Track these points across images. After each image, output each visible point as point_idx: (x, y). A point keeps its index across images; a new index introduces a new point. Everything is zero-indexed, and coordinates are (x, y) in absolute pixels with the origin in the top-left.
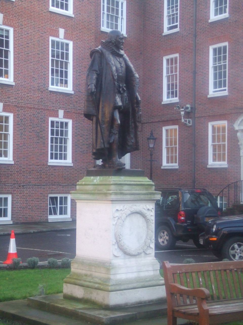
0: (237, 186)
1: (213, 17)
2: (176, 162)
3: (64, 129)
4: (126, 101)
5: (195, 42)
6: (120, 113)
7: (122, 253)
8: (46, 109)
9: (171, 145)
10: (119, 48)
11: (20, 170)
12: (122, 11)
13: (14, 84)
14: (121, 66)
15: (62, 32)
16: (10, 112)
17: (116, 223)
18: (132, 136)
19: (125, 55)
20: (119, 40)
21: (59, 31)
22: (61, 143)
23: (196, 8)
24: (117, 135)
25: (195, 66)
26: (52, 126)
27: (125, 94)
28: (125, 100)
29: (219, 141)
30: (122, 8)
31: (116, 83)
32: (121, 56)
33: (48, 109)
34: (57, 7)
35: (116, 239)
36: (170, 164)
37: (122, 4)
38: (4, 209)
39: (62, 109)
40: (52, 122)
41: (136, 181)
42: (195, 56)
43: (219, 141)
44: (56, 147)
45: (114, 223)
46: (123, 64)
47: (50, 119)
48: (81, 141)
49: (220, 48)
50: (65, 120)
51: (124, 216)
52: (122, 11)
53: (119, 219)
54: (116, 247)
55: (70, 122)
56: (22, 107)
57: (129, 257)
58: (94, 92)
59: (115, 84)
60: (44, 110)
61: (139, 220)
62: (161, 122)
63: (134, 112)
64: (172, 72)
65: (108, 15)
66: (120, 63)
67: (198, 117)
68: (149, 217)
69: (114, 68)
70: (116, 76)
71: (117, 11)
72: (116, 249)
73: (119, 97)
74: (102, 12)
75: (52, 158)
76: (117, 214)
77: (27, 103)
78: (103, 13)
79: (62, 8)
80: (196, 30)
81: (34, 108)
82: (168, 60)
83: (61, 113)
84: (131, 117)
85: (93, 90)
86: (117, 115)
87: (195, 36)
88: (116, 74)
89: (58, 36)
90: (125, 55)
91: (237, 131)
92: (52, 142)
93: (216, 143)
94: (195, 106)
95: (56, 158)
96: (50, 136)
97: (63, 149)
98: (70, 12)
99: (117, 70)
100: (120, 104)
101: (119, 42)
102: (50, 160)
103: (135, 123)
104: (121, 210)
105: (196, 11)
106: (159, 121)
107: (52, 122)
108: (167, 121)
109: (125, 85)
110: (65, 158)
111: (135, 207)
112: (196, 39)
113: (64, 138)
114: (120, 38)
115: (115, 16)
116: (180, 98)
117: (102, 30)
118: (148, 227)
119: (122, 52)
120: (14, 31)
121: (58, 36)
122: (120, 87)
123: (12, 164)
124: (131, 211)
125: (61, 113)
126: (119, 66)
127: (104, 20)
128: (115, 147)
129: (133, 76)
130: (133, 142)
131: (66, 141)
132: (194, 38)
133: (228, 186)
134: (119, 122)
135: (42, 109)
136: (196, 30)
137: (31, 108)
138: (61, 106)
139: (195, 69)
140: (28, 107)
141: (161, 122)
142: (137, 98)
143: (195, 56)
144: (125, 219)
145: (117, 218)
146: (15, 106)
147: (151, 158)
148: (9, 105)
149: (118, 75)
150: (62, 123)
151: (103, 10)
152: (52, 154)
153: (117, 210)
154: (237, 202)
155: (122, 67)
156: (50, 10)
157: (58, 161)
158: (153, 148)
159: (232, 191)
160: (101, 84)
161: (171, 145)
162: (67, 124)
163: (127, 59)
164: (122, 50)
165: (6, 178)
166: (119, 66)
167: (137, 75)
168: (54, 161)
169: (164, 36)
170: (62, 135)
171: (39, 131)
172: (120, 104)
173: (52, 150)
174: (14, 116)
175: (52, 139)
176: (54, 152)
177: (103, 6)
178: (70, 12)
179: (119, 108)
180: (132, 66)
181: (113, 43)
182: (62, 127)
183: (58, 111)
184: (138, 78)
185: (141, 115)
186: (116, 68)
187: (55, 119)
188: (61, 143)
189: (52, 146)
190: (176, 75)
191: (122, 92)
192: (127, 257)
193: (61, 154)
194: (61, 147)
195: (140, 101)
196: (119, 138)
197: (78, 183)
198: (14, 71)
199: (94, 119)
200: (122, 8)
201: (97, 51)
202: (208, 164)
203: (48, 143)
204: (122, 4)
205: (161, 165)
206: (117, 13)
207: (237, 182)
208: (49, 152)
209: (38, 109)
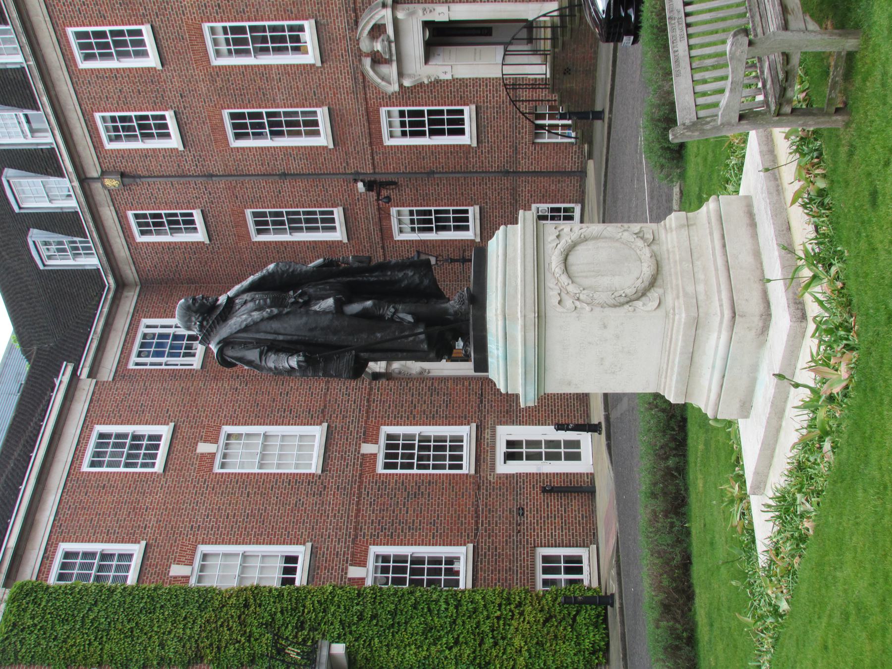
0: (513, 85)
1: (174, 142)
2: (466, 212)
3: (401, 442)
4: (326, 290)
5: (223, 176)
6: (350, 301)
7: (652, 290)
8: (360, 478)
9: (430, 221)
10: (214, 306)
11: (486, 531)
12: (163, 327)
13: (309, 545)
14: (251, 301)
15: (203, 448)
16: (366, 552)
17: (588, 304)
18: (400, 275)
19: (229, 293)
20: (197, 305)
21: (202, 454)
22: (428, 448)
23: (155, 177)
24: (397, 306)
25: (270, 175)
26: (394, 466)
27: (311, 291)
28: (323, 292)
29: (422, 124)
30: (156, 327)
31: (286, 310)
32: (231, 301)
33: (361, 475)
34: (154, 456)
35: (622, 305)
36: (471, 223)
37: (148, 327)
38: (566, 562)
39: (360, 447)
40: (387, 466)
41: (497, 272)
42: (249, 175)
43: (430, 221)
44: (436, 458)
45: (588, 308)
46: (246, 297)
47: (380, 470)
48: (425, 407)
49: (235, 126)
50: (382, 440)
51: (572, 288)
52: (163, 327)
53: (578, 299)
54: (639, 304)
55: (386, 430)
56: (356, 529)
57: (659, 277)
58: (304, 356)
59: (288, 313)
60: (361, 482)
61: (579, 258)
62: (383, 243)
63: (349, 271)
64: (282, 223)
65: (171, 355)
66: (245, 303)
67: (374, 169)
68: (574, 236)
69: (256, 315)
70: (271, 311)
71: (161, 336)
72: (644, 305)
73: (316, 304)
74: (163, 367)
75: (460, 467)
76: (569, 302)
77: (348, 518)
78: (166, 365)
79: (157, 447)
80: (198, 176)
81: (358, 503)
82: (259, 232)
83: (367, 448)
84: (361, 279)
85: (301, 358)
86: (355, 308)
87: (212, 176)
88: (268, 310)
89: (213, 455)
90: (231, 293)
91: (401, 86)
92: (426, 467)
93: (427, 129)
94: (352, 174)
95: (460, 458)
96: (415, 471)
97: (440, 444)
98: (165, 431)
99: (259, 308)
100: (330, 302)
101: (202, 305)
102: (465, 471)
103: (371, 270)
104: (559, 294)
105: (161, 177)
106: (383, 248)
107: (387, 466)
108: (381, 230)
109: (291, 293)
110: (460, 439)
111: (554, 265)
112: (217, 176)
113: (419, 441)
114: (194, 304)
115: (173, 340)
116: (335, 205)
117: (199, 367)
118: (596, 238)
119: (222, 299)
120: (204, 542)
121: (213, 455)
122: (296, 302)
123: (474, 546)
124: (560, 272)
125: (367, 448)
126: (250, 305)
127: (179, 363)
128: (423, 308)
129: (271, 275)
130: (414, 274)
131: (425, 439)
132: (214, 179)
133: (513, 102)
134: (369, 303)
135: (359, 488)
136: (198, 176)
137: (358, 510)
138: (353, 448)
139: (276, 175)
140: (357, 516)
141: (383, 243)
142: (319, 267)
143: (249, 175)
144: (580, 285)
145: (577, 303)
146: (353, 543)
147: (457, 261)
148: (353, 555)
149: (269, 307)
150: (388, 447)
151: (161, 364)
152: (451, 467)
153: (560, 302)
154: (546, 84)
155: (253, 300)
156: (161, 471)
157: (465, 453)
158: (437, 258)
159: (524, 94)
160: (288, 342)
161: (430, 221)
162: (390, 437)
163: (237, 288)
164: (217, 300)
165: (503, 559)
166: (250, 305)
167: (271, 267)
168: (464, 462)
169: (210, 240)
170: (412, 447)
171: (405, 494)
172: (330, 302)
173: (443, 467)
174: (375, 544)
175: (420, 467)
176: (447, 462)
177: (152, 364)
178: (165, 431)
179: (340, 305)
180: (251, 279)
181: (204, 319)
182: (396, 447)
183: (363, 455)
184: (277, 265)
185: (354, 257)
186: (256, 310)
187: (381, 461)
188: (428, 448)
189: (435, 467)
190: (288, 213)
191: (306, 298)
192: (659, 282)
193: (452, 448)
194: (436, 448)
195: (325, 259)
196: (404, 303)
197: (503, 391)
198: (284, 544)
199: (363, 355)
200: (156, 327)
201: (221, 351)
202: (470, 146)
203: (430, 474)
204: (148, 327)
205: (473, 241)
206: (166, 336)
207: (505, 85)
208: (447, 471)
209: (360, 494)
